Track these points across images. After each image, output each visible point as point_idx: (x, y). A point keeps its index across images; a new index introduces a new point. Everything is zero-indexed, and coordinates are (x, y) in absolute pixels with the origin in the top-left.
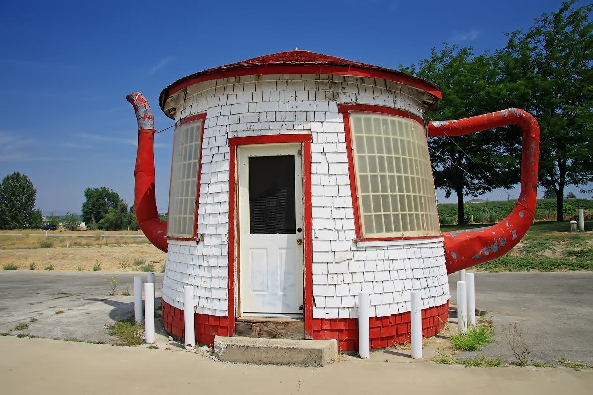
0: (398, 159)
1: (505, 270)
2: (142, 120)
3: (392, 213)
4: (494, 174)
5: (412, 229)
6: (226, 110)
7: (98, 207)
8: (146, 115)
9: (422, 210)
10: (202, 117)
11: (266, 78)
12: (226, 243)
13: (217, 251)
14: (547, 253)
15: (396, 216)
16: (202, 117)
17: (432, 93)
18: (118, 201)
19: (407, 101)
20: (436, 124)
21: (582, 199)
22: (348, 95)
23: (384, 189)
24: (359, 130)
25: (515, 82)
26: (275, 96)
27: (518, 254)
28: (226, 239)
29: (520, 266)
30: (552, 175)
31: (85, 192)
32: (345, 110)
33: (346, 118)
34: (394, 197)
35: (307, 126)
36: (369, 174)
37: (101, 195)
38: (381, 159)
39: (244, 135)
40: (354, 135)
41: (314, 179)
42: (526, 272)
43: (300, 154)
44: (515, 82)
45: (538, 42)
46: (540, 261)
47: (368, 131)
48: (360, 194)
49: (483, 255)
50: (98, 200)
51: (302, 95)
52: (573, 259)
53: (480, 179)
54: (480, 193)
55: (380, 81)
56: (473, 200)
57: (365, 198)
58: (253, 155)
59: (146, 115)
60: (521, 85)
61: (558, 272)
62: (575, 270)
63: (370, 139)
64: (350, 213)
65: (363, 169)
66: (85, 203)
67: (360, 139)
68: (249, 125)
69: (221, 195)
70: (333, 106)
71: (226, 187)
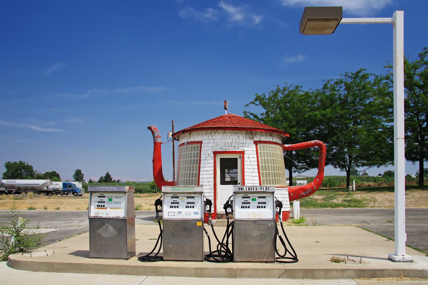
0: (273, 160)
1: (314, 208)
2: (156, 138)
3: (271, 178)
4: (312, 161)
5: (278, 184)
6: (212, 141)
7: (16, 176)
8: (158, 136)
9: (281, 178)
10: (201, 142)
11: (227, 131)
12: (213, 188)
13: (210, 191)
14: (335, 201)
15: (273, 179)
16: (201, 142)
17: (286, 135)
18: (32, 171)
19: (277, 138)
20: (286, 146)
21: (371, 176)
22: (257, 137)
23: (269, 170)
24: (260, 150)
25: (325, 110)
26: (231, 137)
27: (320, 201)
28: (213, 186)
29: (321, 206)
30: (344, 162)
31: (5, 164)
32: (256, 143)
33: (256, 145)
34: (272, 173)
35: (243, 148)
36: (264, 165)
37: (18, 167)
38: (268, 160)
39: (220, 150)
40: (259, 151)
41: (245, 167)
42: (324, 209)
43: (240, 157)
44: (325, 110)
45: (341, 87)
46: (330, 204)
47: (264, 150)
48: (261, 172)
49: (303, 195)
50: (16, 171)
51: (241, 137)
52: (346, 203)
53: (304, 163)
54: (303, 172)
55: (268, 133)
56: (298, 176)
57: (263, 173)
58: (222, 157)
59: (158, 136)
60: (328, 112)
61: (338, 208)
62: (346, 208)
63: (264, 153)
64: (258, 178)
65: (262, 163)
66: (6, 172)
67: (261, 153)
68: (221, 147)
69: (210, 171)
70: (252, 142)
71: (213, 168)
